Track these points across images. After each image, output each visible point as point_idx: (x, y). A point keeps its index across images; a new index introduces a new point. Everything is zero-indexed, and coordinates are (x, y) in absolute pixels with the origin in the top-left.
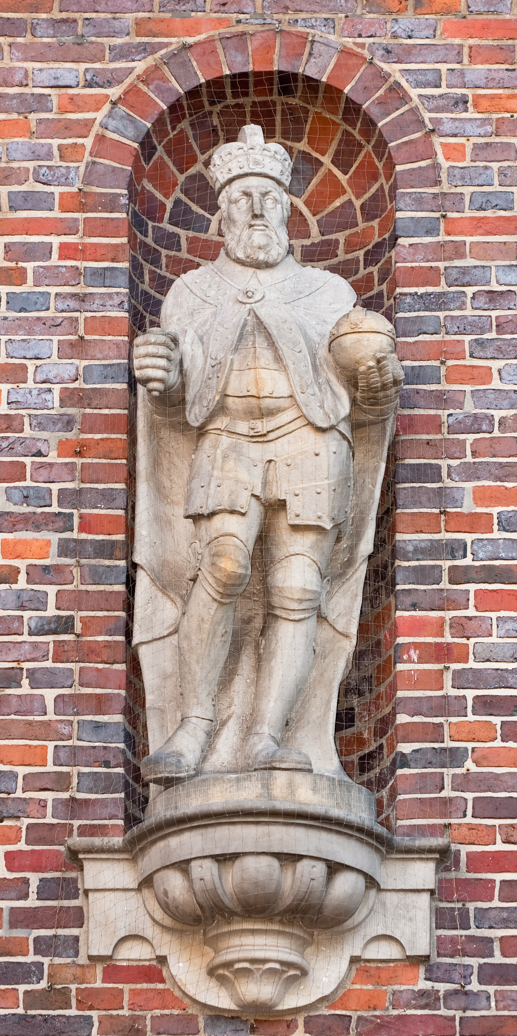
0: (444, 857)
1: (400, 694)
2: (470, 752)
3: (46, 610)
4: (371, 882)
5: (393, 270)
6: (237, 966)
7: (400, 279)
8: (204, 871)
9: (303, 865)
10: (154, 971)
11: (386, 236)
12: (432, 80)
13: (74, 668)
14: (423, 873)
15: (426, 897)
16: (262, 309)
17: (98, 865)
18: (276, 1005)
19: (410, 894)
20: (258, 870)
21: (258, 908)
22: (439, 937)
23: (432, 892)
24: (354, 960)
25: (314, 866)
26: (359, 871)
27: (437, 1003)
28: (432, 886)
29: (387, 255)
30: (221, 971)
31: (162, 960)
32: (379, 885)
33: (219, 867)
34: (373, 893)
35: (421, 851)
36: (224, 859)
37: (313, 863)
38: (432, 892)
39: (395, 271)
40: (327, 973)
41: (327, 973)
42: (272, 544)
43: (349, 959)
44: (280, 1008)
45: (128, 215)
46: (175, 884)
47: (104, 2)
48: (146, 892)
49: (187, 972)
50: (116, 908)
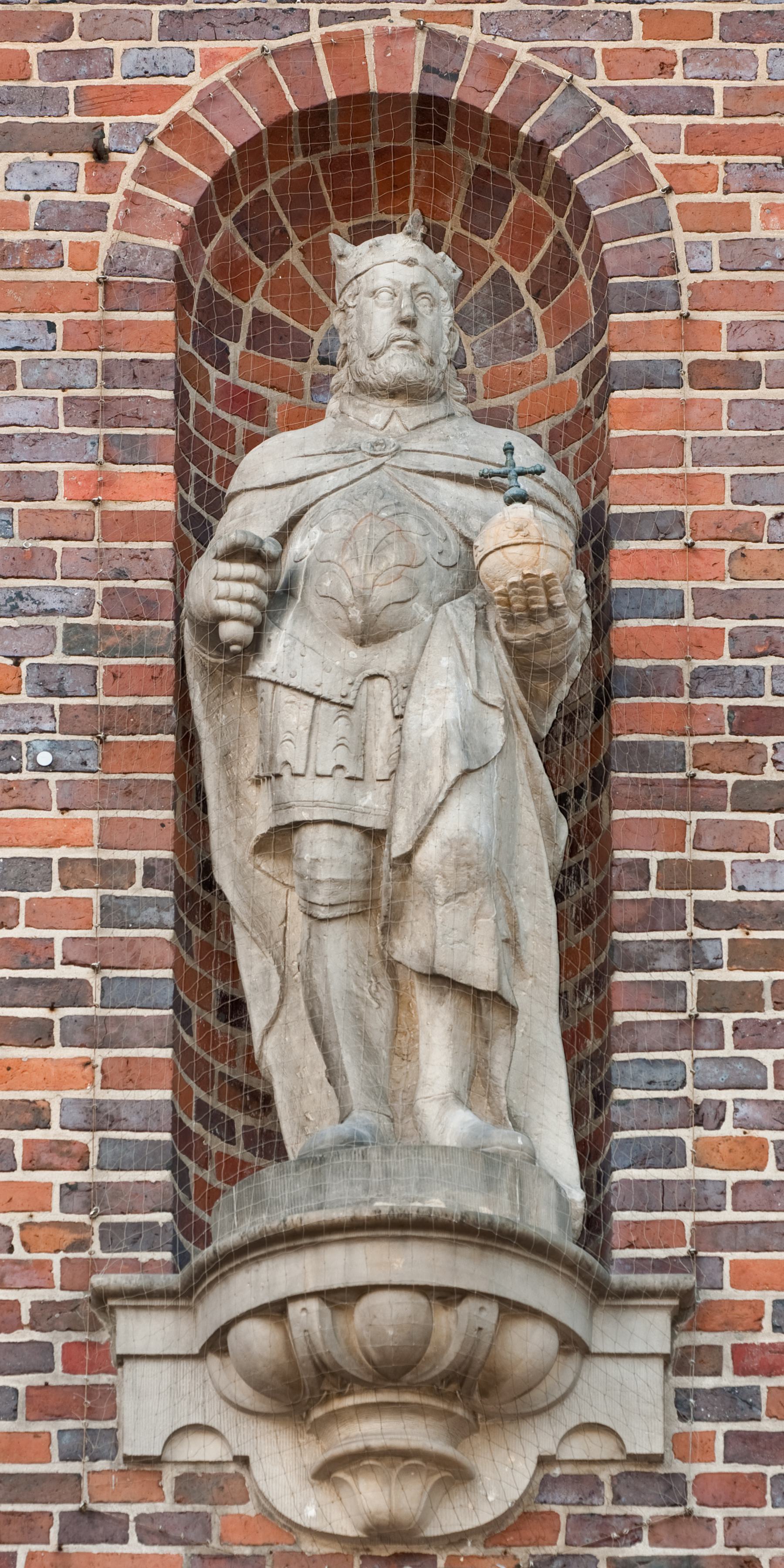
0: (685, 1310)
1: (620, 1018)
2: (685, 377)
3: (71, 14)
4: (572, 1344)
8: (308, 1317)
9: (468, 1307)
10: (228, 1481)
12: (710, 233)
13: (96, 588)
14: (651, 1330)
15: (657, 1366)
16: (394, 474)
17: (132, 1314)
21: (394, 1372)
23: (666, 1359)
24: (543, 1461)
25: (482, 1309)
26: (552, 1321)
31: (244, 1461)
33: (332, 1316)
34: (574, 1361)
35: (652, 1294)
36: (341, 1298)
38: (666, 1359)
40: (504, 1475)
41: (504, 1475)
43: (536, 1461)
44: (432, 1531)
46: (257, 1338)
47: (3, 1268)
48: (213, 1361)
49: (281, 1470)
50: (161, 1398)
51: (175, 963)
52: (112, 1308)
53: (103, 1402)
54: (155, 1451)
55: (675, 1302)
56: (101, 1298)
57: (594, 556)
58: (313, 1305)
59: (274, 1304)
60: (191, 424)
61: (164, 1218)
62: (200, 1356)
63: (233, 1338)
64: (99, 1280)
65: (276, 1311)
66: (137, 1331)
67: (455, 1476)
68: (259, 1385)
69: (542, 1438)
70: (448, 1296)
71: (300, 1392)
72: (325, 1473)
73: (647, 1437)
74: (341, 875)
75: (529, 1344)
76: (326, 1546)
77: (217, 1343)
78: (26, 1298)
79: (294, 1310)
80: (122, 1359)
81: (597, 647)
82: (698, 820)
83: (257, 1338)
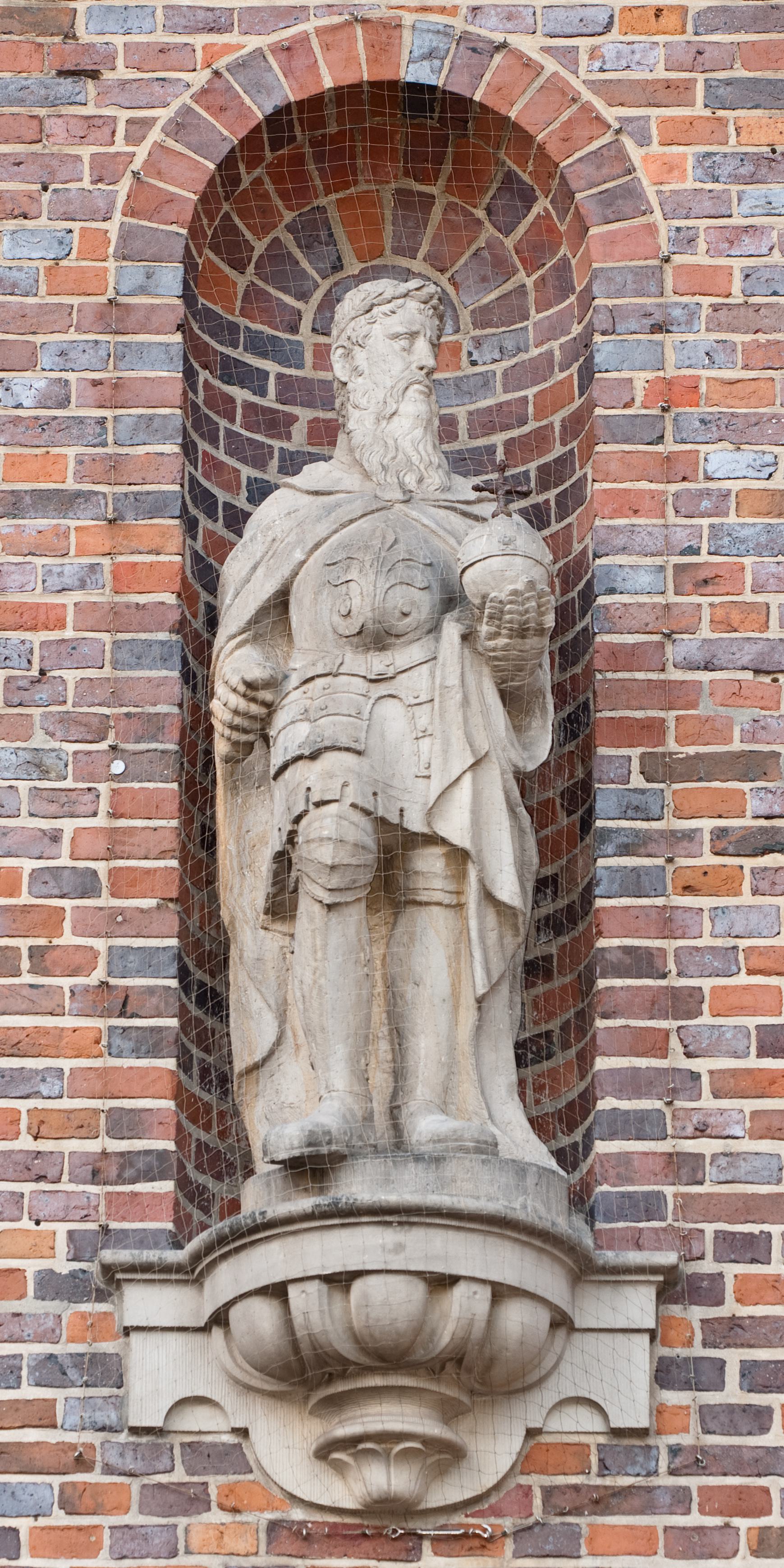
0: (672, 1287)
4: (561, 1322)
5: (589, 495)
6: (361, 1446)
7: (600, 432)
9: (460, 1291)
10: (232, 1455)
11: (574, 594)
14: (638, 1305)
18: (419, 1503)
19: (620, 1337)
20: (389, 1303)
21: (391, 1359)
22: (661, 1359)
23: (652, 1334)
24: (531, 1433)
27: (675, 611)
28: (652, 1325)
29: (578, 474)
30: (336, 1455)
31: (243, 1432)
32: (572, 1322)
35: (641, 1270)
36: (340, 1281)
37: (475, 1287)
38: (652, 1334)
39: (592, 496)
40: (494, 1451)
42: (389, 1494)
44: (422, 1506)
45: (182, 486)
49: (284, 1448)
51: (180, 932)
52: (119, 1280)
53: (107, 1372)
54: (157, 1421)
55: (661, 1278)
56: (108, 1270)
57: (579, 1065)
58: (314, 1287)
59: (275, 1285)
60: (200, 401)
61: (167, 1186)
62: (205, 1329)
63: (234, 1314)
64: (108, 1255)
65: (278, 1291)
66: (142, 1303)
67: (445, 1456)
68: (262, 1369)
69: (533, 1411)
70: (441, 1283)
71: (307, 1374)
72: (325, 1452)
73: (632, 1408)
74: (344, 857)
75: (518, 1319)
76: (267, 1382)
77: (220, 1319)
78: (31, 1267)
79: (293, 1292)
80: (127, 1331)
81: (582, 1096)
82: (676, 950)
83: (259, 1320)
